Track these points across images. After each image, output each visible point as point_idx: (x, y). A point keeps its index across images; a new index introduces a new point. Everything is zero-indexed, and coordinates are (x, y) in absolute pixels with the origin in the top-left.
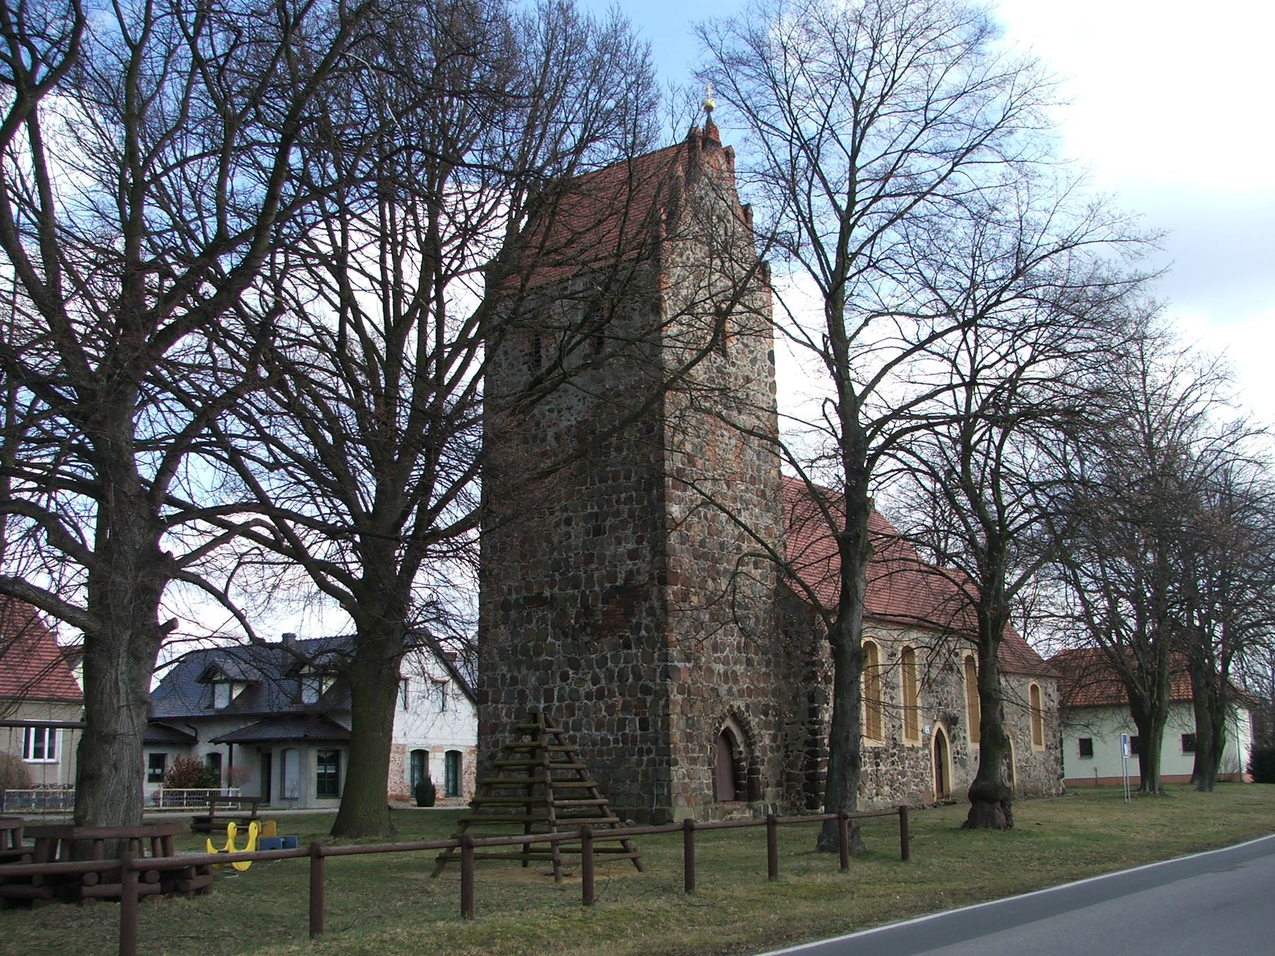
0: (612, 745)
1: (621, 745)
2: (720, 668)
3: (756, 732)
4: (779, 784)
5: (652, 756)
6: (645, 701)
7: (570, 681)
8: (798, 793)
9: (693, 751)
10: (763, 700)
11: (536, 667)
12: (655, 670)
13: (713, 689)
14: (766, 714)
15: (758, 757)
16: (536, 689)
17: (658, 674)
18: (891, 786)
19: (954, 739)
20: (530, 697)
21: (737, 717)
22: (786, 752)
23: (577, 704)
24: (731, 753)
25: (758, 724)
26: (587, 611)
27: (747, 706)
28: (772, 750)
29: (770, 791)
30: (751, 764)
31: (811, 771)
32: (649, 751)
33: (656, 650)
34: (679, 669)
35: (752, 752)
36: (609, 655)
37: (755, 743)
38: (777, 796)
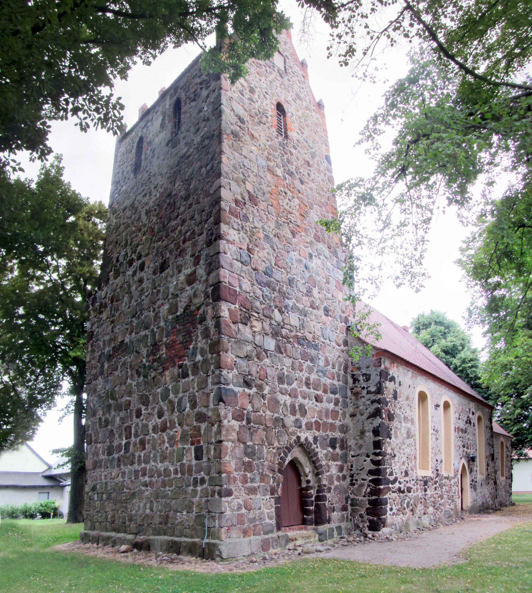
0: (173, 476)
1: (179, 475)
2: (287, 399)
3: (324, 463)
4: (344, 509)
5: (205, 486)
6: (199, 427)
7: (142, 417)
8: (361, 516)
9: (253, 480)
10: (332, 434)
11: (119, 408)
12: (208, 395)
13: (277, 420)
14: (334, 448)
15: (325, 485)
16: (120, 427)
17: (211, 399)
18: (434, 506)
19: (471, 471)
20: (117, 436)
21: (305, 447)
22: (352, 480)
23: (147, 438)
24: (300, 482)
25: (326, 455)
26: (156, 346)
27: (315, 439)
28: (338, 479)
29: (335, 515)
30: (318, 492)
31: (374, 498)
32: (203, 481)
33: (210, 373)
34: (235, 394)
35: (319, 481)
36: (170, 387)
37: (322, 473)
38: (342, 519)
